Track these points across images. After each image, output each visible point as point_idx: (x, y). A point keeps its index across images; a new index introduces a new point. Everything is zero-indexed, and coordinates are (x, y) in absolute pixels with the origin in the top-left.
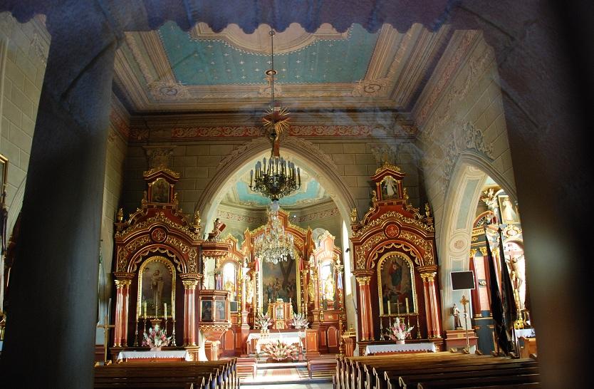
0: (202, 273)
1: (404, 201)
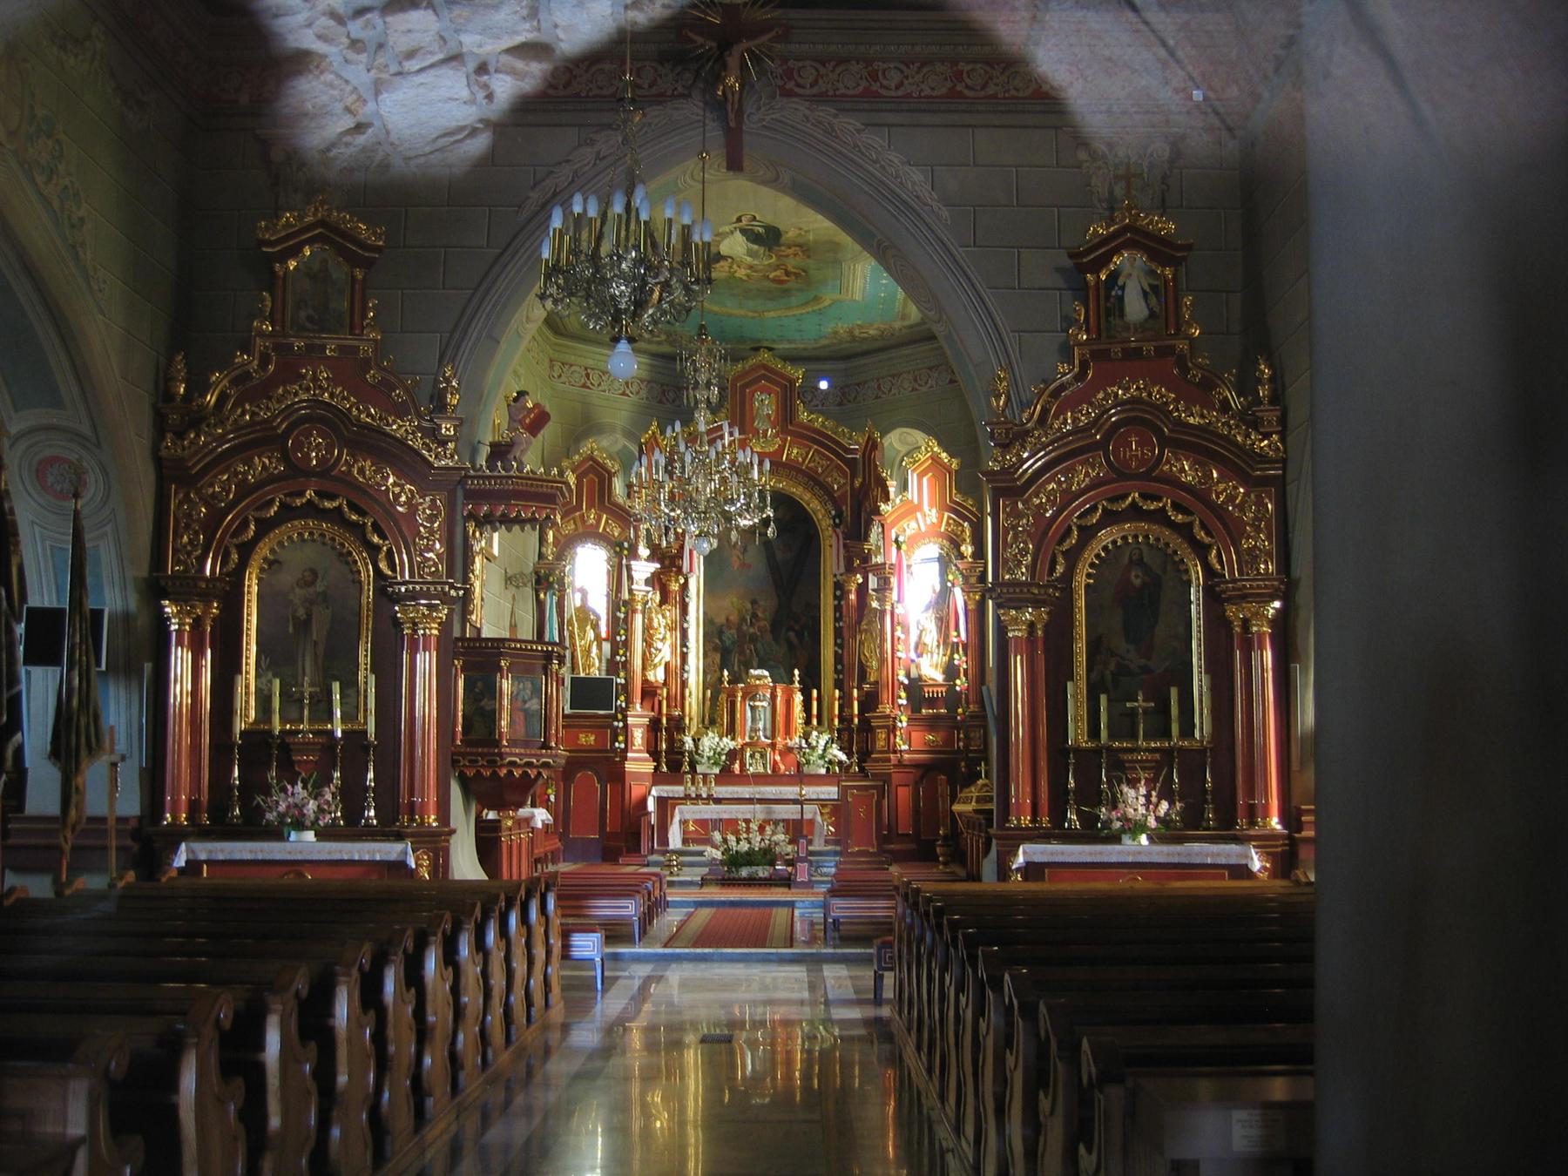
0: (466, 580)
1: (1183, 346)
